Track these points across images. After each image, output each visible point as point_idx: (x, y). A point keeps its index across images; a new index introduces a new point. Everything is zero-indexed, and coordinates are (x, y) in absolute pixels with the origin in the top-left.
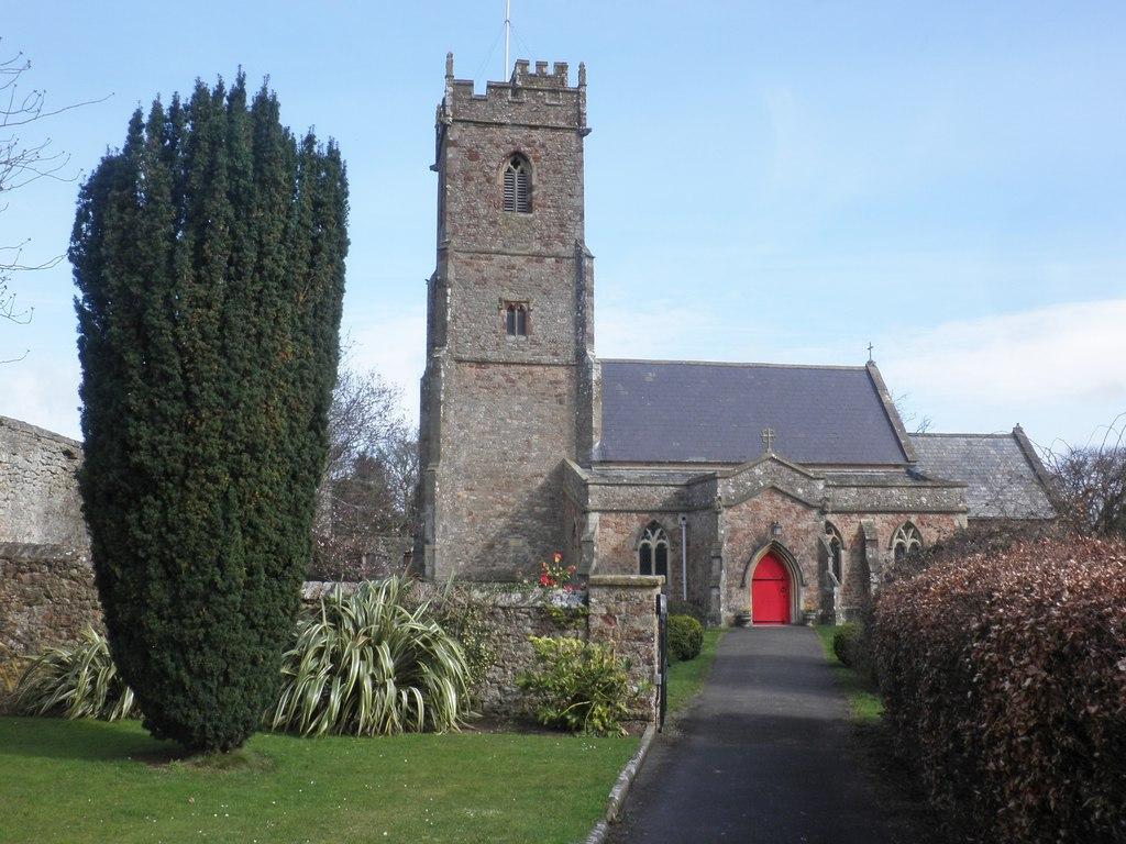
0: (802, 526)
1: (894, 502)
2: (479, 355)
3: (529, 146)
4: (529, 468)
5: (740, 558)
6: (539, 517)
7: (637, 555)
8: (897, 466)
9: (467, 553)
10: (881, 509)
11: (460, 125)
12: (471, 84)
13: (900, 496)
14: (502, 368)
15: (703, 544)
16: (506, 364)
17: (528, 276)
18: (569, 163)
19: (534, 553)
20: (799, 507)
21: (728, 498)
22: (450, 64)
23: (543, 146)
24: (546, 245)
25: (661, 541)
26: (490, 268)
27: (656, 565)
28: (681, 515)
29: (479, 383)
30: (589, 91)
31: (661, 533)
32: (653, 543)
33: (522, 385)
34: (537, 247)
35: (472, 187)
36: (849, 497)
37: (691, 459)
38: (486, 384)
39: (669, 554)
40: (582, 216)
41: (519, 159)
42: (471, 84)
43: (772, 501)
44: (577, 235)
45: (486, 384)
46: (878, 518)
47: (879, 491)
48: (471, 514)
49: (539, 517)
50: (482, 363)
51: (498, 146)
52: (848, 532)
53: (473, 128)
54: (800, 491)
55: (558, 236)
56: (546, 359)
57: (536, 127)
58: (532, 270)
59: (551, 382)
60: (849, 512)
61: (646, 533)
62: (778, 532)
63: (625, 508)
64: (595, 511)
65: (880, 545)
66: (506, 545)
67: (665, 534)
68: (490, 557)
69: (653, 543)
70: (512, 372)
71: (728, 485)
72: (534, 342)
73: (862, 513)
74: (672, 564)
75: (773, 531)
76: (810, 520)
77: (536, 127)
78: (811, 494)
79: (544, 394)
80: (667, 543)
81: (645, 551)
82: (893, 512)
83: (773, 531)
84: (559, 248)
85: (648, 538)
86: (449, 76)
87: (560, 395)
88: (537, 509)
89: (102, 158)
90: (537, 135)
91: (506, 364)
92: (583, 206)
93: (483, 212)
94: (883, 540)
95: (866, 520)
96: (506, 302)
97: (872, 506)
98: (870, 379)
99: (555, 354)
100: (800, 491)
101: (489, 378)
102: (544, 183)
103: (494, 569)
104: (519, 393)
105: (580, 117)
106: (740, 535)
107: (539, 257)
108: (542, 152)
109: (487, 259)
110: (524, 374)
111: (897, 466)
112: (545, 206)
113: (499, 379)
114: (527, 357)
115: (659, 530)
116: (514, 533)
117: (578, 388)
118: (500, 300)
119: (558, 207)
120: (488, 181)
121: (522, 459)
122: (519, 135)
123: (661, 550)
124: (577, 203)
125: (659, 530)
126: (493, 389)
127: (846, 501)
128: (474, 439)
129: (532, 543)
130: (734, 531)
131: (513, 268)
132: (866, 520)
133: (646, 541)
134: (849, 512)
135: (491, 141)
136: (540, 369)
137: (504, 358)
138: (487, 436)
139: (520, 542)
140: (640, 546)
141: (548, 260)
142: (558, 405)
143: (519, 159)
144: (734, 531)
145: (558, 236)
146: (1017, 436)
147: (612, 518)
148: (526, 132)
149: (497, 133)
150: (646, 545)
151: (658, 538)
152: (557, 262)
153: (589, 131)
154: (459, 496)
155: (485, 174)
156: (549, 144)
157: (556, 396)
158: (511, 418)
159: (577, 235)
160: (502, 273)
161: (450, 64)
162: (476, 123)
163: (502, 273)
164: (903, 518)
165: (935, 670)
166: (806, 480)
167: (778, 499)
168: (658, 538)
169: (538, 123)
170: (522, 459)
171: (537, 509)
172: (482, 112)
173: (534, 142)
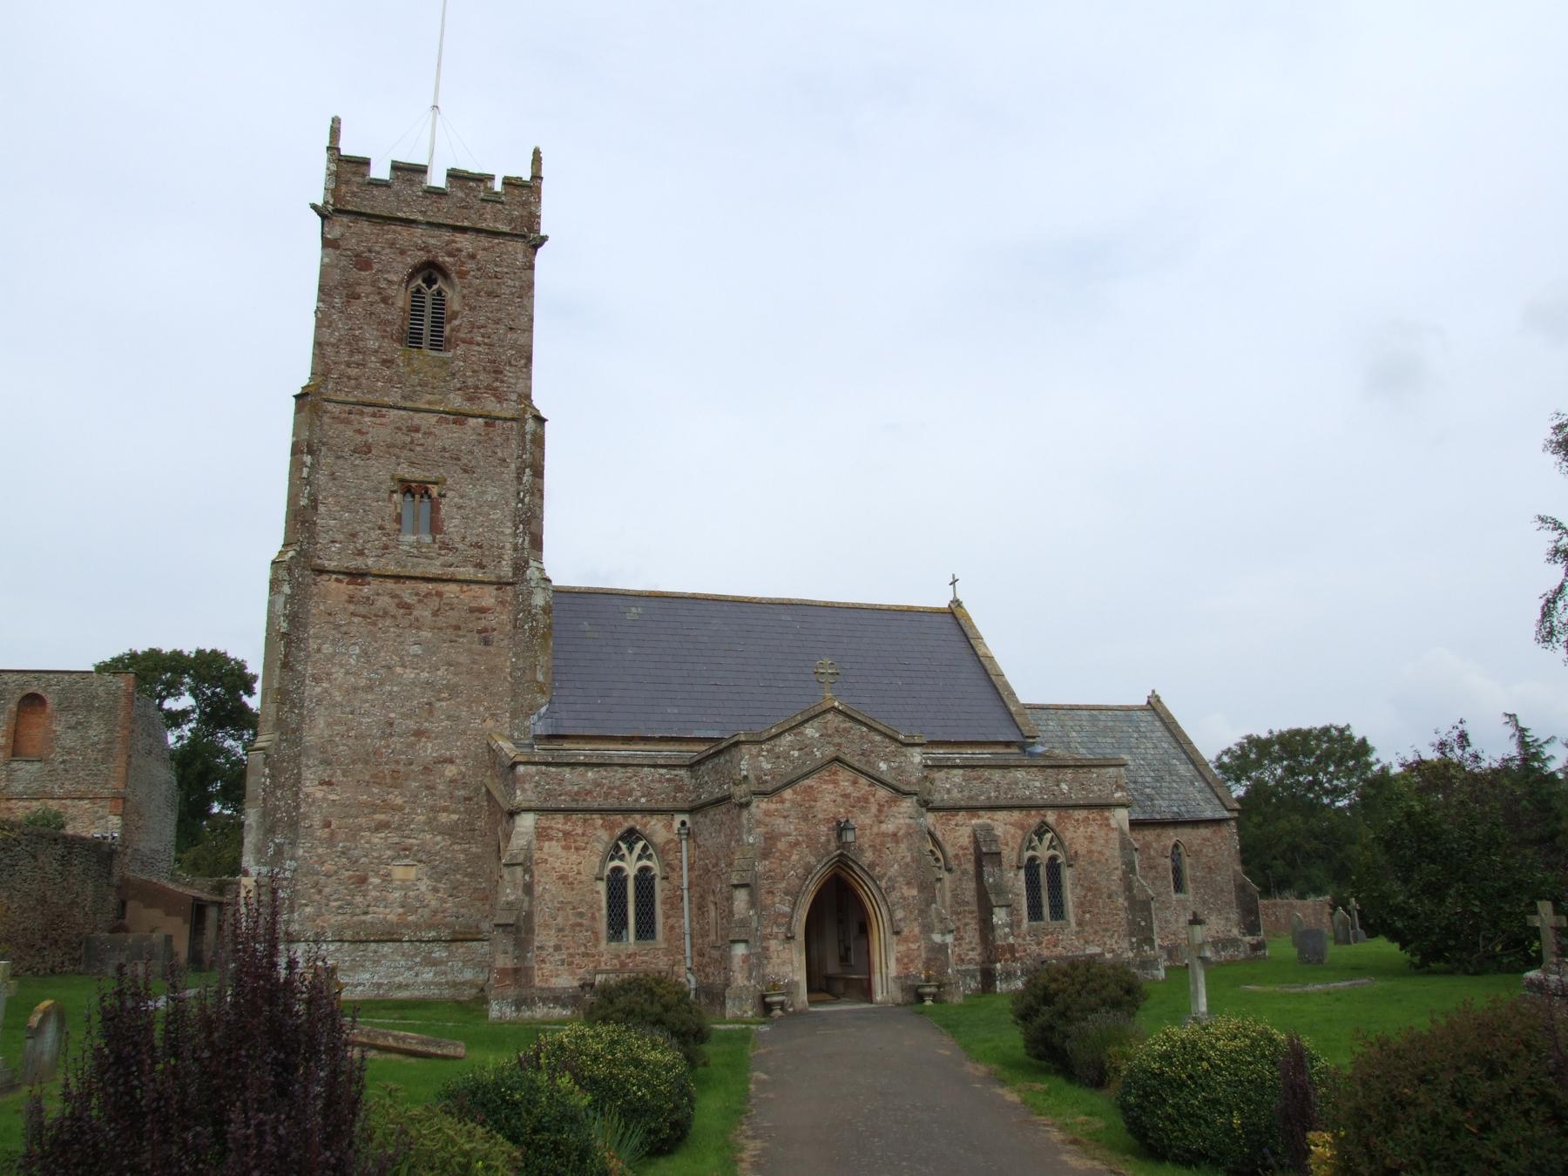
0: (888, 827)
1: (1022, 793)
2: (357, 563)
3: (450, 254)
4: (429, 750)
5: (783, 885)
6: (450, 831)
7: (602, 887)
8: (1008, 744)
9: (320, 892)
10: (1003, 803)
11: (345, 219)
12: (366, 162)
13: (1029, 783)
14: (390, 584)
15: (716, 865)
16: (397, 578)
17: (439, 444)
18: (510, 283)
19: (436, 890)
20: (882, 793)
21: (759, 779)
22: (335, 132)
23: (472, 257)
24: (470, 399)
25: (644, 862)
26: (379, 430)
27: (625, 897)
28: (679, 818)
29: (352, 607)
30: (546, 187)
31: (645, 848)
32: (631, 867)
33: (424, 613)
34: (457, 401)
35: (357, 308)
36: (950, 786)
37: (697, 734)
38: (362, 609)
39: (659, 885)
40: (529, 359)
41: (436, 275)
42: (366, 162)
43: (836, 783)
44: (520, 387)
45: (362, 609)
46: (1001, 815)
47: (997, 775)
48: (328, 825)
49: (450, 831)
50: (357, 576)
51: (403, 252)
52: (959, 834)
53: (365, 226)
54: (883, 766)
55: (488, 387)
56: (467, 572)
57: (463, 230)
58: (449, 436)
59: (472, 610)
60: (954, 809)
61: (618, 848)
62: (850, 837)
63: (581, 805)
64: (528, 810)
65: (1004, 860)
66: (387, 878)
67: (651, 851)
68: (359, 899)
69: (631, 867)
70: (406, 591)
71: (759, 755)
72: (445, 546)
73: (972, 810)
74: (664, 903)
75: (840, 836)
76: (903, 814)
77: (463, 230)
78: (900, 770)
79: (457, 628)
80: (654, 865)
81: (616, 881)
82: (1020, 808)
83: (840, 836)
84: (491, 405)
85: (622, 858)
86: (333, 148)
87: (485, 630)
88: (443, 817)
89: (225, 653)
90: (465, 242)
91: (397, 578)
92: (531, 346)
93: (372, 344)
94: (1009, 855)
95: (980, 821)
96: (402, 481)
97: (989, 798)
98: (954, 616)
99: (481, 566)
100: (883, 766)
101: (368, 601)
102: (472, 309)
103: (368, 918)
104: (417, 625)
105: (533, 220)
106: (781, 845)
107: (460, 417)
108: (471, 265)
109: (374, 415)
110: (428, 595)
111: (1008, 744)
112: (471, 343)
113: (384, 601)
114: (435, 570)
115: (641, 844)
116: (398, 857)
117: (516, 620)
118: (392, 478)
119: (491, 345)
120: (385, 300)
121: (419, 734)
122: (436, 240)
123: (645, 880)
124: (522, 341)
125: (641, 844)
126: (371, 619)
127: (948, 791)
128: (338, 699)
129: (437, 875)
130: (771, 838)
131: (417, 430)
132: (984, 819)
133: (616, 863)
134: (954, 809)
135: (392, 244)
136: (453, 587)
137: (393, 569)
138: (362, 695)
139: (412, 873)
140: (607, 872)
141: (472, 421)
142: (482, 647)
143: (436, 275)
144: (771, 838)
145: (488, 387)
146: (1154, 706)
147: (558, 822)
148: (447, 235)
149: (403, 235)
150: (618, 870)
151: (640, 858)
152: (487, 424)
153: (544, 239)
154: (308, 795)
155: (380, 291)
156: (480, 255)
157: (479, 632)
158: (404, 666)
159: (520, 387)
160: (402, 438)
161: (335, 132)
162: (369, 217)
163: (402, 438)
164: (1034, 820)
165: (257, 946)
166: (893, 748)
167: (845, 778)
168: (640, 858)
169: (466, 224)
170: (419, 734)
171: (443, 817)
172: (382, 204)
173: (459, 250)
